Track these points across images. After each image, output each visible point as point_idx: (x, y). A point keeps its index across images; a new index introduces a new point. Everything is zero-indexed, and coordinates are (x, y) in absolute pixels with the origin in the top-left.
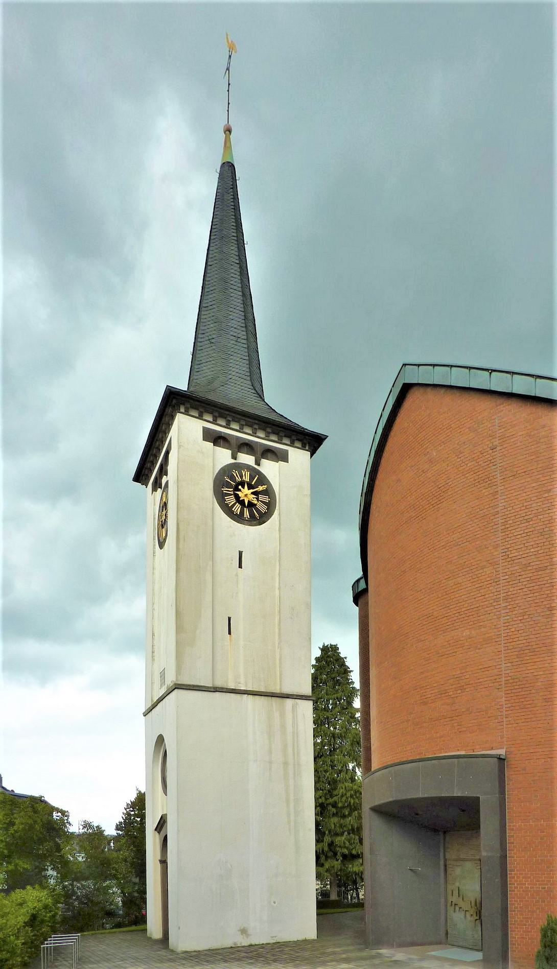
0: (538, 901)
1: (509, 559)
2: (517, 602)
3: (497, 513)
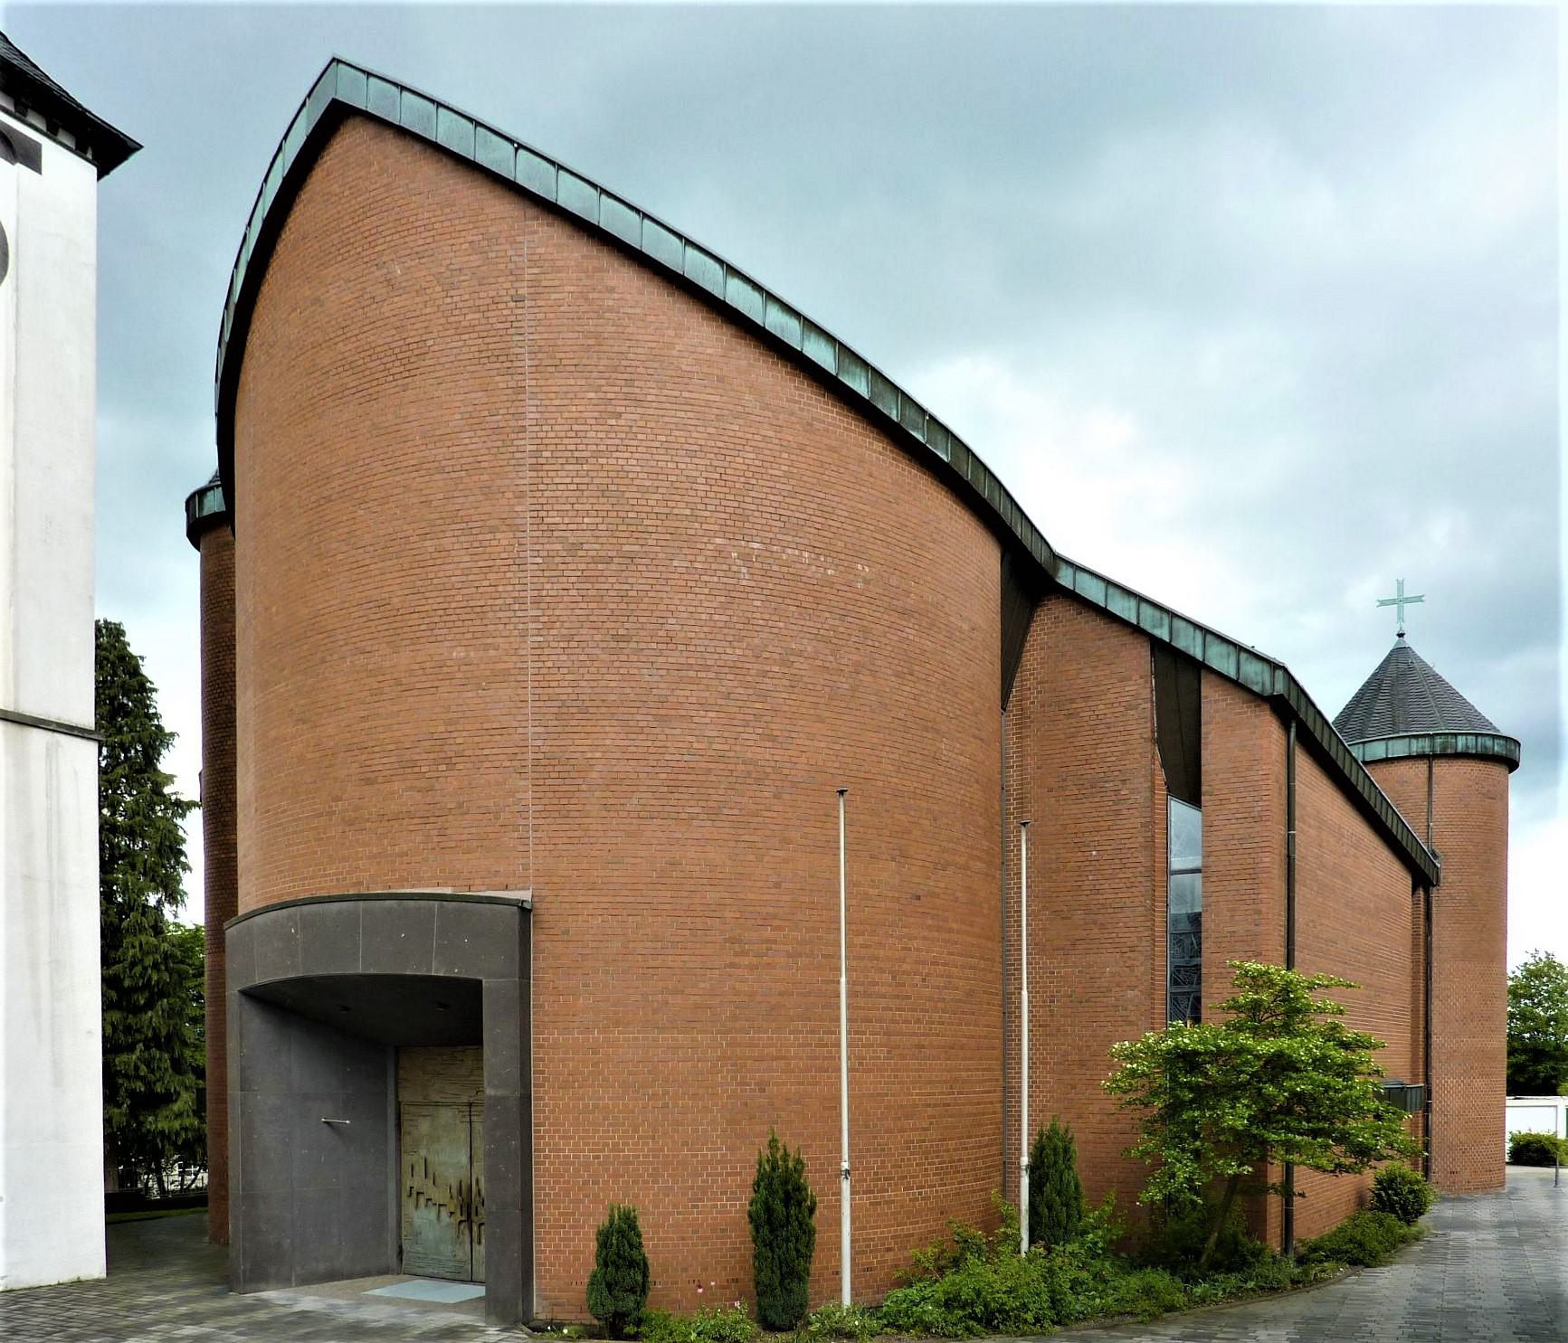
0: (586, 1183)
1: (545, 527)
2: (557, 612)
3: (523, 429)
